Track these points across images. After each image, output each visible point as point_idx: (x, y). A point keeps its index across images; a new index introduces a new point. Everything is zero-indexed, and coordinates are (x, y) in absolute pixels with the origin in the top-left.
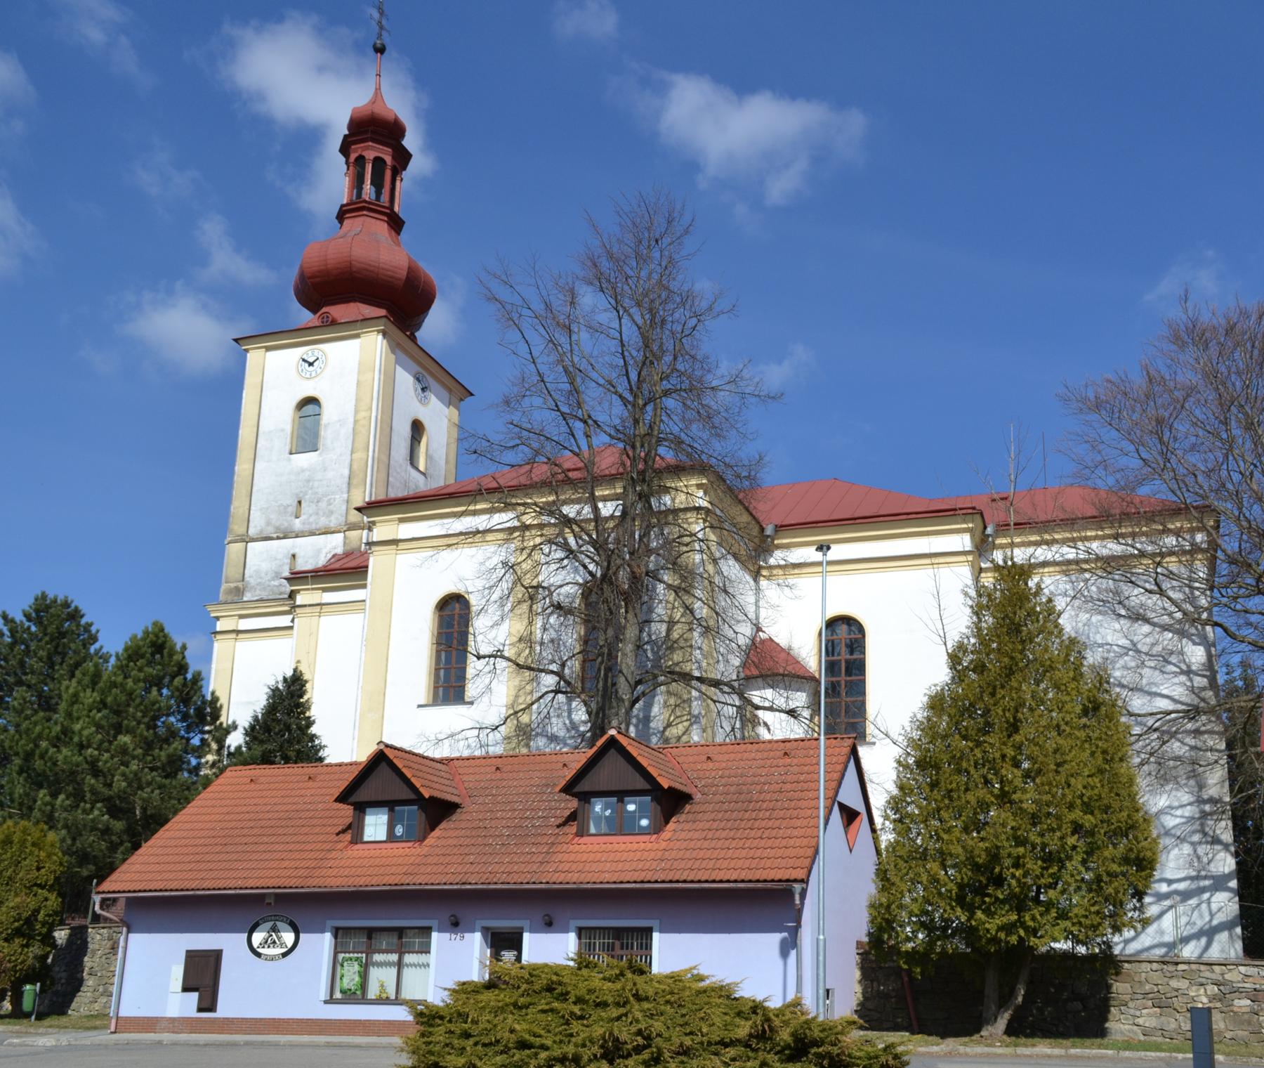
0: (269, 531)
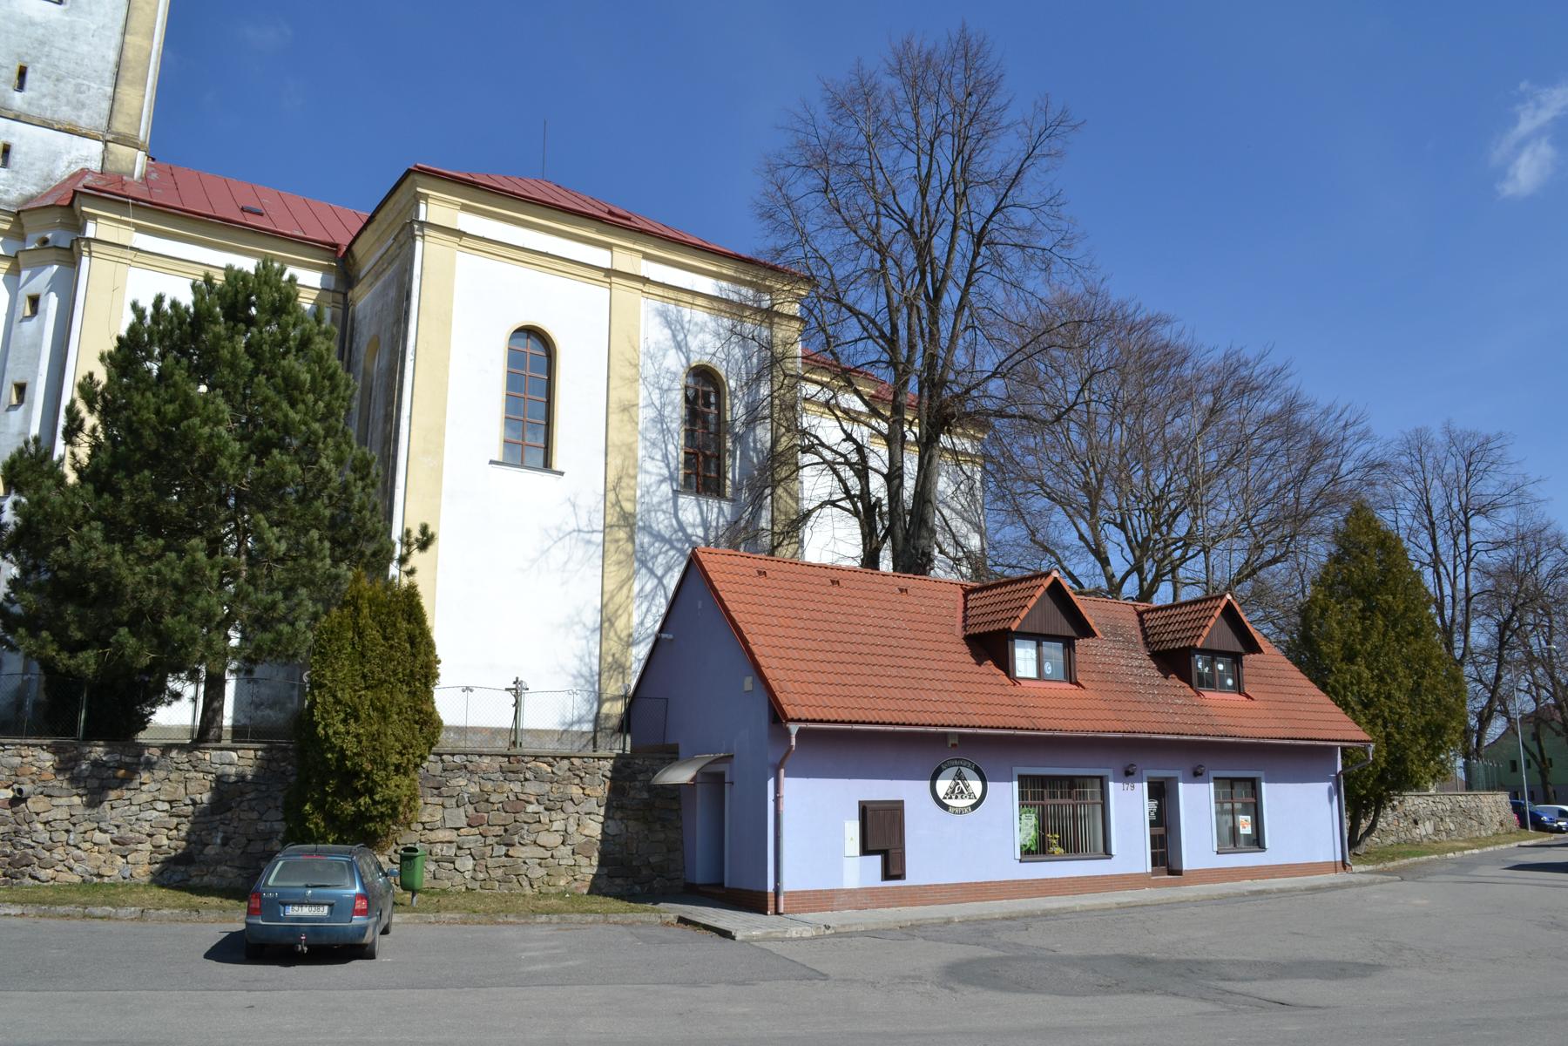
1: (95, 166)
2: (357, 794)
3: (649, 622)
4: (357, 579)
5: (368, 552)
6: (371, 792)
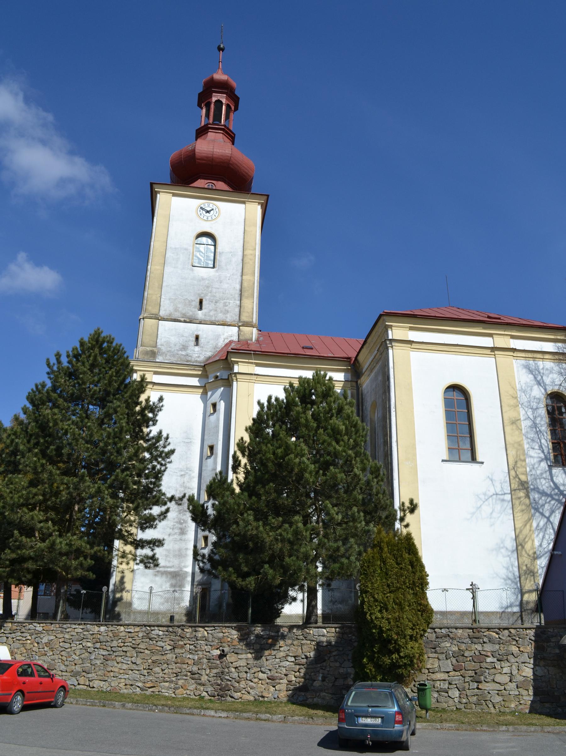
0: (177, 315)
1: (235, 338)
2: (391, 653)
3: (545, 544)
4: (379, 532)
5: (383, 517)
6: (398, 651)
